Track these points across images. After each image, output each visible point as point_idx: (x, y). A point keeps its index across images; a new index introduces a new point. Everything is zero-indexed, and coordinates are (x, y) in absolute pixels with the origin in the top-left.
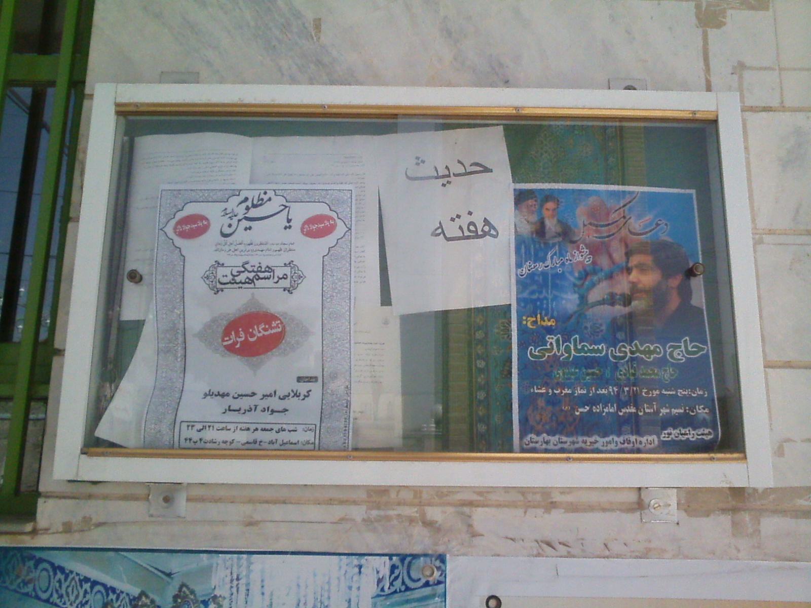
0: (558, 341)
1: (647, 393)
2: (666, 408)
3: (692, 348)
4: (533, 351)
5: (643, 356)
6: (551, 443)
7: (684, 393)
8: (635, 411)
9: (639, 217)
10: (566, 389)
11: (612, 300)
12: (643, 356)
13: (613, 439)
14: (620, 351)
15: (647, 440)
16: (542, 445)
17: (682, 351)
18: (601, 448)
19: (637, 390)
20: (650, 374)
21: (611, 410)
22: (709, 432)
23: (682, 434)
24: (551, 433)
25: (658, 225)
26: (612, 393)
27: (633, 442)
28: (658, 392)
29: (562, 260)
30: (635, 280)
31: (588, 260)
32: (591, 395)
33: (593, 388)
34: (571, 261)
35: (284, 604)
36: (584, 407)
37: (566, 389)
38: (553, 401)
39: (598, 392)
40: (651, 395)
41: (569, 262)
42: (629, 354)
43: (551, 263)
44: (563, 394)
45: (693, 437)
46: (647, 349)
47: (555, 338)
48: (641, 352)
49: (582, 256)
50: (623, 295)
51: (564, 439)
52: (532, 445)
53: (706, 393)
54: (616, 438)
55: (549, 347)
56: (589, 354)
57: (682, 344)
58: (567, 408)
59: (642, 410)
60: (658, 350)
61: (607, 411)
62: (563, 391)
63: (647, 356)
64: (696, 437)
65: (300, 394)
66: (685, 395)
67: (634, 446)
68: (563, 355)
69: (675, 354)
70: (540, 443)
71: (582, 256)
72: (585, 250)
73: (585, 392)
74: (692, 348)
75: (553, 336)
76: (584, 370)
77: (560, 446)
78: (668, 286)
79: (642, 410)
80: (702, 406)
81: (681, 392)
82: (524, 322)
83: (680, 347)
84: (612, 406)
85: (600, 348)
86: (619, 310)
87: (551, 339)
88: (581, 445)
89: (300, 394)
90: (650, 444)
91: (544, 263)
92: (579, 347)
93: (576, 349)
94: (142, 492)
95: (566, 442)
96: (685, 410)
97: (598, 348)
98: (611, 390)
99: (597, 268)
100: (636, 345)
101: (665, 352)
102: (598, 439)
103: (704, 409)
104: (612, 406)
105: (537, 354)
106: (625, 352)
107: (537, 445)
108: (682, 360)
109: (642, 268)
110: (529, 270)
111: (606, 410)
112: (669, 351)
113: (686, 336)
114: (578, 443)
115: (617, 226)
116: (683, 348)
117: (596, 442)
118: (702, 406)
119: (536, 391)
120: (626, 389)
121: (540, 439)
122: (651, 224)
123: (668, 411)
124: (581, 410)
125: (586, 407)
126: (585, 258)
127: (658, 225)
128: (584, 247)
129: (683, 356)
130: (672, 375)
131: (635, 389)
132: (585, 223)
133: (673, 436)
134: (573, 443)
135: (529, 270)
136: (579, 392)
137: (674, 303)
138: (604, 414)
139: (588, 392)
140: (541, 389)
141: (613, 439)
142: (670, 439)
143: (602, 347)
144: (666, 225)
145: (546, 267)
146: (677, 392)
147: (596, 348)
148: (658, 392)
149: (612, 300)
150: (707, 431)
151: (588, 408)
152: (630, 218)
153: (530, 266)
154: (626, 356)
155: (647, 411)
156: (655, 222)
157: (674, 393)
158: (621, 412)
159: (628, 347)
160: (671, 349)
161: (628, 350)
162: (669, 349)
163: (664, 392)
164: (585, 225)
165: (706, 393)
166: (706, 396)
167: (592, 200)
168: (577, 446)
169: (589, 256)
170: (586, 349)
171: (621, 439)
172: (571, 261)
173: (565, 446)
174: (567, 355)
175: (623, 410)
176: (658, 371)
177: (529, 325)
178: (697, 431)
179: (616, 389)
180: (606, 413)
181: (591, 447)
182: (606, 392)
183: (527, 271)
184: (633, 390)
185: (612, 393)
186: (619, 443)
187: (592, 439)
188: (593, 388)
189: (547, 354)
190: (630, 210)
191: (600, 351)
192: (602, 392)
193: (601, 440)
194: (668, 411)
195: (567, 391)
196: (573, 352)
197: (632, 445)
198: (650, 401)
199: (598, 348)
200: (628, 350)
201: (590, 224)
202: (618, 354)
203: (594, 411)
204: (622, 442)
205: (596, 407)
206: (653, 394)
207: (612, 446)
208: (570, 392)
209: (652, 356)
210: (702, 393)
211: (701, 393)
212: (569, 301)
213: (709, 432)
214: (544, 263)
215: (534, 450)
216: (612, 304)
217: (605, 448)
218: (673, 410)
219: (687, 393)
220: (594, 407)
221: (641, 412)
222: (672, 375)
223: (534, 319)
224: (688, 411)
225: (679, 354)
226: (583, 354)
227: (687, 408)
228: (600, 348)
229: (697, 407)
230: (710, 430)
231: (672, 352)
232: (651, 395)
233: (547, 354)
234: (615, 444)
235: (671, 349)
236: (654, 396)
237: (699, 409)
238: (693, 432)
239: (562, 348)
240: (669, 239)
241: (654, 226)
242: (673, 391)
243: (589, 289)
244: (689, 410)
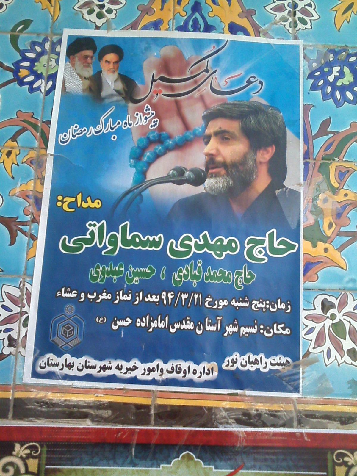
0: (101, 229)
1: (211, 304)
2: (234, 325)
3: (278, 245)
4: (67, 241)
5: (212, 252)
6: (75, 368)
7: (259, 306)
8: (192, 328)
9: (226, 72)
10: (104, 294)
11: (178, 177)
12: (212, 252)
13: (158, 366)
14: (182, 245)
15: (204, 368)
16: (62, 369)
17: (265, 248)
18: (140, 377)
19: (198, 298)
20: (219, 278)
21: (161, 325)
22: (287, 361)
23: (250, 363)
24: (77, 353)
25: (249, 82)
26: (165, 302)
27: (185, 370)
28: (225, 303)
29: (119, 123)
30: (213, 152)
31: (153, 124)
32: (136, 303)
33: (141, 294)
34: (130, 125)
35: (73, 370)
36: (124, 319)
37: (104, 294)
38: (89, 309)
39: (146, 300)
40: (215, 307)
41: (128, 126)
42: (194, 250)
43: (104, 126)
44: (99, 301)
45: (265, 368)
46: (219, 243)
47: (98, 225)
48: (210, 247)
49: (146, 119)
50: (195, 171)
51: (92, 362)
52: (48, 369)
53: (289, 307)
54: (162, 365)
55: (88, 236)
56: (140, 247)
57: (267, 239)
58: (101, 319)
59: (202, 327)
60: (233, 245)
61: (156, 326)
62: (100, 296)
63: (218, 252)
64: (269, 367)
65: (122, 366)
66: (261, 308)
67: (185, 376)
68: (105, 247)
69: (255, 252)
70: (60, 367)
71: (146, 119)
72: (151, 111)
73: (129, 299)
74: (278, 245)
75: (95, 222)
76: (132, 269)
77: (86, 371)
78: (255, 160)
79: (202, 327)
80: (283, 325)
81: (256, 305)
82: (59, 204)
83: (263, 242)
84: (163, 319)
85: (157, 240)
86: (188, 190)
87: (93, 227)
88: (114, 371)
89: (122, 366)
90: (208, 374)
91: (95, 127)
92: (129, 238)
93: (125, 241)
94: (29, 272)
95: (94, 367)
96: (259, 329)
97: (154, 239)
98: (164, 297)
99: (164, 133)
100: (205, 237)
101: (242, 247)
102: (138, 364)
103: (284, 329)
104: (163, 319)
105: (71, 245)
106: (189, 247)
107: (56, 369)
108: (264, 259)
109: (223, 136)
110: (74, 136)
111: (153, 325)
112: (247, 247)
113: (192, 260)
114: (110, 368)
115: (196, 82)
116: (267, 244)
117: (135, 368)
118: (283, 325)
119: (64, 295)
120: (184, 296)
121: (61, 360)
122: (240, 81)
123: (236, 329)
124: (120, 323)
125: (128, 319)
126: (150, 122)
127: (249, 82)
128: (149, 107)
129: (266, 255)
130: (247, 280)
131: (196, 296)
132: (155, 78)
133: (238, 365)
134: (104, 368)
135: (74, 136)
136: (122, 298)
137: (262, 182)
138: (150, 330)
139: (134, 299)
140: (71, 292)
141: (158, 366)
142: (234, 368)
143: (160, 238)
144: (261, 83)
145: (96, 132)
146: (251, 304)
147: (151, 239)
148: (225, 303)
149: (178, 177)
150: (284, 360)
151: (130, 321)
152: (215, 72)
153: (75, 131)
154: (191, 251)
155: (208, 328)
156: (247, 79)
157: (247, 305)
158: (173, 328)
159: (194, 240)
160: (251, 245)
161: (192, 244)
162: (248, 244)
163: (233, 303)
164: (153, 80)
165: (289, 307)
166: (289, 311)
167: (167, 51)
168: (108, 373)
169: (155, 120)
170: (137, 240)
171: (168, 366)
172: (130, 125)
173: (93, 372)
174: (110, 248)
175: (177, 326)
176: (229, 274)
177: (65, 207)
178: (271, 359)
179: (170, 296)
180: (154, 328)
181: (128, 376)
182: (157, 300)
183: (71, 137)
184: (194, 297)
185: (165, 302)
186: (165, 371)
187: (130, 365)
188: (141, 294)
189: (85, 246)
190: (217, 61)
191: (157, 244)
192: (151, 300)
193: (142, 367)
194: (236, 329)
195: (105, 296)
196: (120, 244)
197: (182, 374)
198: (214, 314)
199: (154, 239)
200: (192, 244)
201: (162, 79)
202: (180, 249)
203: (138, 325)
204: (170, 370)
205: (142, 321)
206: (219, 305)
207: (155, 375)
208: (109, 297)
209: (224, 253)
210: (284, 308)
211: (283, 306)
212: (121, 178)
213: (287, 361)
214: (95, 127)
215: (51, 375)
216: (180, 183)
217: (145, 377)
218: (242, 329)
219: (263, 306)
220: (139, 320)
221: (200, 329)
222: (247, 280)
223: (73, 199)
224: (262, 331)
225: (260, 252)
226: (132, 247)
227: (262, 327)
228: (157, 240)
229: (275, 325)
230: (289, 360)
231: (253, 247)
232: (215, 307)
233: (85, 246)
234: (159, 373)
235: (251, 245)
236: (221, 307)
237: (278, 329)
238: (266, 360)
239: (106, 239)
240: (264, 102)
241: (245, 84)
242: (246, 302)
243: (149, 164)
244: (264, 329)
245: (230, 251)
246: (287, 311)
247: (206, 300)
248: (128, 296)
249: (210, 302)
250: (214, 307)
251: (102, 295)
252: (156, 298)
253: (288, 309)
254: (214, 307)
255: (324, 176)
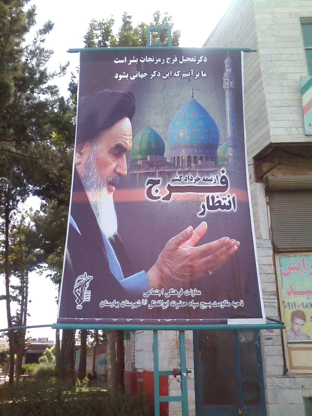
44: (198, 63)
160: (150, 185)
162: (147, 185)
166: (163, 63)
231: (151, 188)
235: (150, 185)
245: (221, 209)
246: (197, 63)
247: (167, 59)
248: (152, 59)
249: (169, 60)
250: (172, 63)
251: (174, 59)
252: (194, 59)
253: (163, 61)
254: (172, 63)
255: (61, 136)
